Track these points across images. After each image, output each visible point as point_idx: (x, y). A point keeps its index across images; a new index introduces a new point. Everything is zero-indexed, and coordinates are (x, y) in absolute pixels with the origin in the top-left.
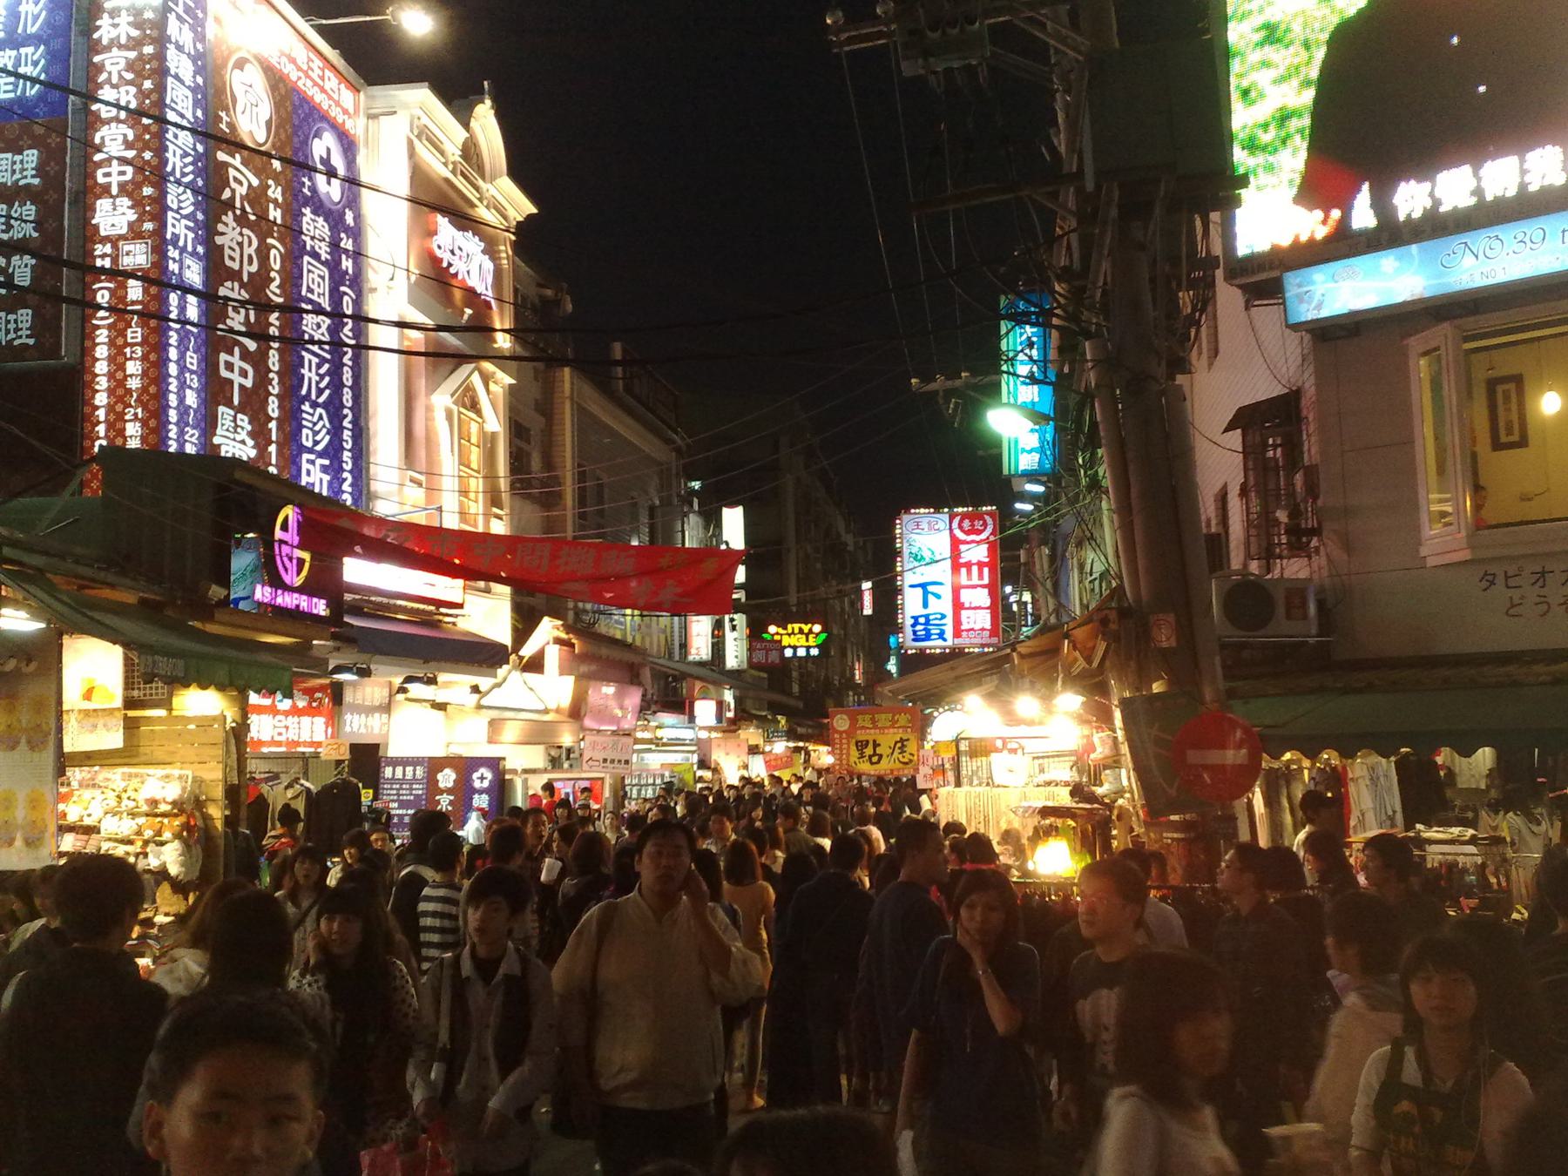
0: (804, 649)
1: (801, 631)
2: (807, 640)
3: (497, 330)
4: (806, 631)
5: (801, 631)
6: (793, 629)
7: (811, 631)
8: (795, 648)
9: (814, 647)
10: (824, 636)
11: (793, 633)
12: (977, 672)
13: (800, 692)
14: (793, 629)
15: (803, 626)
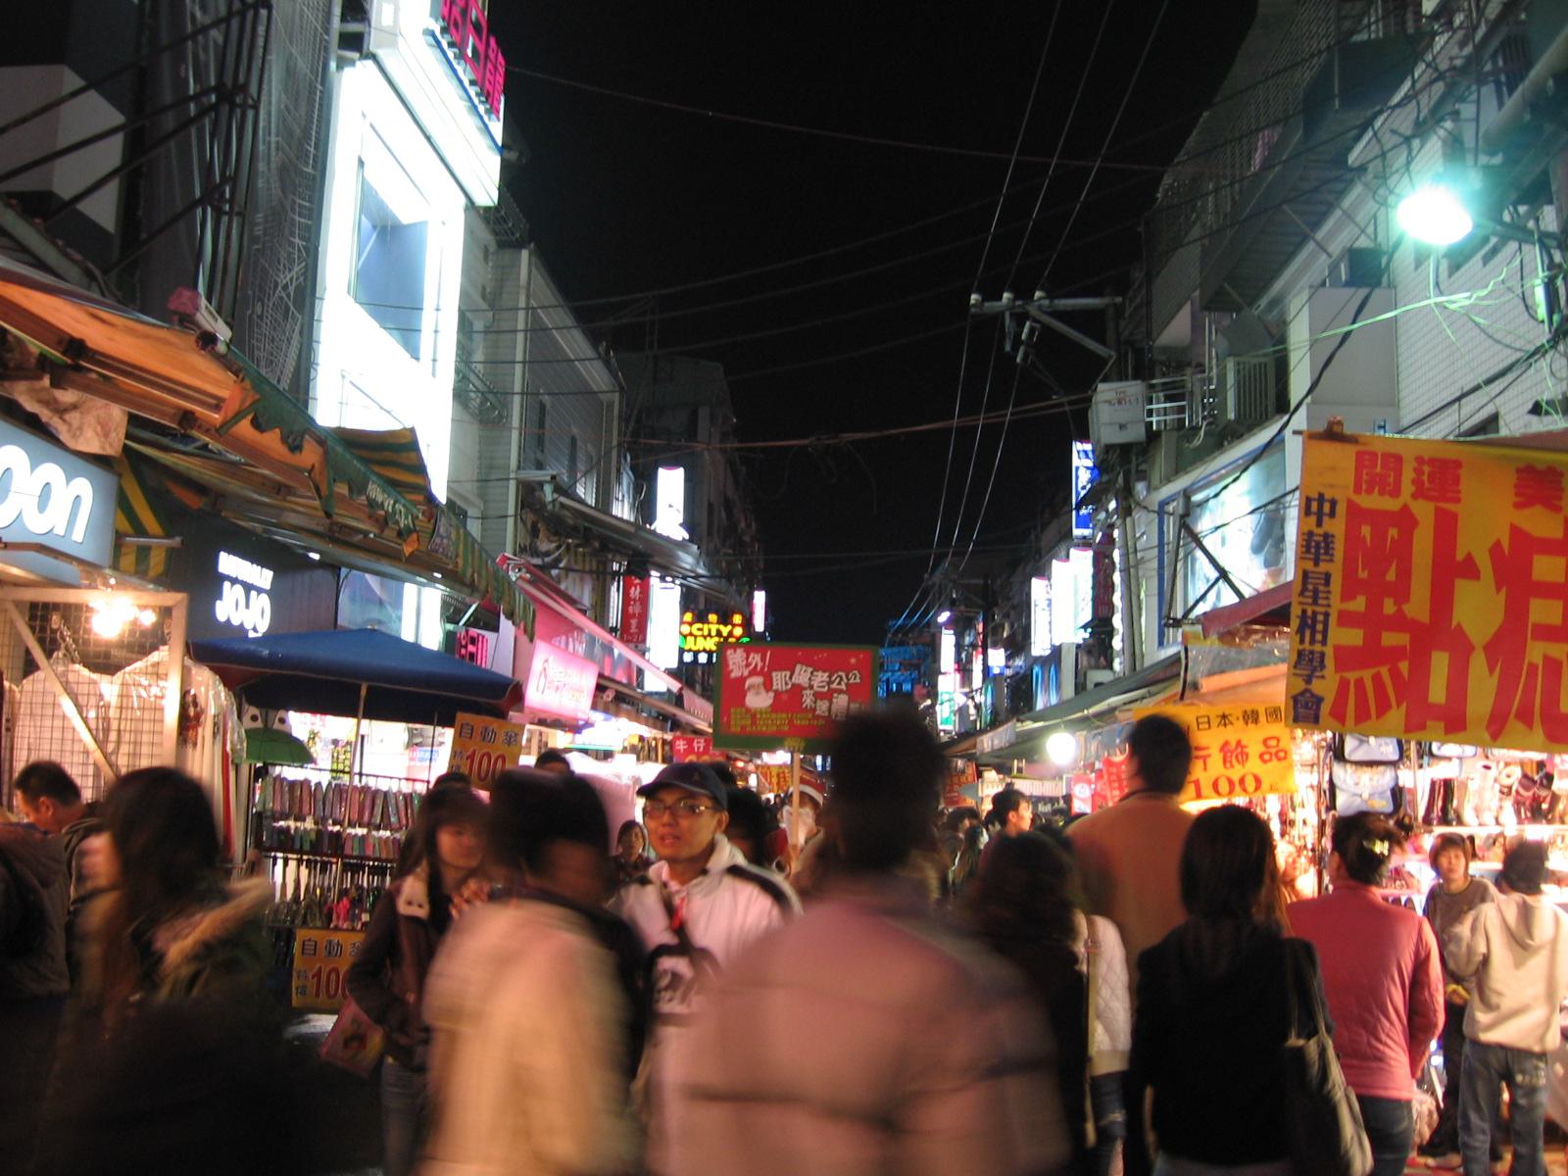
4: (725, 634)
6: (710, 630)
11: (710, 635)
14: (710, 630)
15: (722, 627)
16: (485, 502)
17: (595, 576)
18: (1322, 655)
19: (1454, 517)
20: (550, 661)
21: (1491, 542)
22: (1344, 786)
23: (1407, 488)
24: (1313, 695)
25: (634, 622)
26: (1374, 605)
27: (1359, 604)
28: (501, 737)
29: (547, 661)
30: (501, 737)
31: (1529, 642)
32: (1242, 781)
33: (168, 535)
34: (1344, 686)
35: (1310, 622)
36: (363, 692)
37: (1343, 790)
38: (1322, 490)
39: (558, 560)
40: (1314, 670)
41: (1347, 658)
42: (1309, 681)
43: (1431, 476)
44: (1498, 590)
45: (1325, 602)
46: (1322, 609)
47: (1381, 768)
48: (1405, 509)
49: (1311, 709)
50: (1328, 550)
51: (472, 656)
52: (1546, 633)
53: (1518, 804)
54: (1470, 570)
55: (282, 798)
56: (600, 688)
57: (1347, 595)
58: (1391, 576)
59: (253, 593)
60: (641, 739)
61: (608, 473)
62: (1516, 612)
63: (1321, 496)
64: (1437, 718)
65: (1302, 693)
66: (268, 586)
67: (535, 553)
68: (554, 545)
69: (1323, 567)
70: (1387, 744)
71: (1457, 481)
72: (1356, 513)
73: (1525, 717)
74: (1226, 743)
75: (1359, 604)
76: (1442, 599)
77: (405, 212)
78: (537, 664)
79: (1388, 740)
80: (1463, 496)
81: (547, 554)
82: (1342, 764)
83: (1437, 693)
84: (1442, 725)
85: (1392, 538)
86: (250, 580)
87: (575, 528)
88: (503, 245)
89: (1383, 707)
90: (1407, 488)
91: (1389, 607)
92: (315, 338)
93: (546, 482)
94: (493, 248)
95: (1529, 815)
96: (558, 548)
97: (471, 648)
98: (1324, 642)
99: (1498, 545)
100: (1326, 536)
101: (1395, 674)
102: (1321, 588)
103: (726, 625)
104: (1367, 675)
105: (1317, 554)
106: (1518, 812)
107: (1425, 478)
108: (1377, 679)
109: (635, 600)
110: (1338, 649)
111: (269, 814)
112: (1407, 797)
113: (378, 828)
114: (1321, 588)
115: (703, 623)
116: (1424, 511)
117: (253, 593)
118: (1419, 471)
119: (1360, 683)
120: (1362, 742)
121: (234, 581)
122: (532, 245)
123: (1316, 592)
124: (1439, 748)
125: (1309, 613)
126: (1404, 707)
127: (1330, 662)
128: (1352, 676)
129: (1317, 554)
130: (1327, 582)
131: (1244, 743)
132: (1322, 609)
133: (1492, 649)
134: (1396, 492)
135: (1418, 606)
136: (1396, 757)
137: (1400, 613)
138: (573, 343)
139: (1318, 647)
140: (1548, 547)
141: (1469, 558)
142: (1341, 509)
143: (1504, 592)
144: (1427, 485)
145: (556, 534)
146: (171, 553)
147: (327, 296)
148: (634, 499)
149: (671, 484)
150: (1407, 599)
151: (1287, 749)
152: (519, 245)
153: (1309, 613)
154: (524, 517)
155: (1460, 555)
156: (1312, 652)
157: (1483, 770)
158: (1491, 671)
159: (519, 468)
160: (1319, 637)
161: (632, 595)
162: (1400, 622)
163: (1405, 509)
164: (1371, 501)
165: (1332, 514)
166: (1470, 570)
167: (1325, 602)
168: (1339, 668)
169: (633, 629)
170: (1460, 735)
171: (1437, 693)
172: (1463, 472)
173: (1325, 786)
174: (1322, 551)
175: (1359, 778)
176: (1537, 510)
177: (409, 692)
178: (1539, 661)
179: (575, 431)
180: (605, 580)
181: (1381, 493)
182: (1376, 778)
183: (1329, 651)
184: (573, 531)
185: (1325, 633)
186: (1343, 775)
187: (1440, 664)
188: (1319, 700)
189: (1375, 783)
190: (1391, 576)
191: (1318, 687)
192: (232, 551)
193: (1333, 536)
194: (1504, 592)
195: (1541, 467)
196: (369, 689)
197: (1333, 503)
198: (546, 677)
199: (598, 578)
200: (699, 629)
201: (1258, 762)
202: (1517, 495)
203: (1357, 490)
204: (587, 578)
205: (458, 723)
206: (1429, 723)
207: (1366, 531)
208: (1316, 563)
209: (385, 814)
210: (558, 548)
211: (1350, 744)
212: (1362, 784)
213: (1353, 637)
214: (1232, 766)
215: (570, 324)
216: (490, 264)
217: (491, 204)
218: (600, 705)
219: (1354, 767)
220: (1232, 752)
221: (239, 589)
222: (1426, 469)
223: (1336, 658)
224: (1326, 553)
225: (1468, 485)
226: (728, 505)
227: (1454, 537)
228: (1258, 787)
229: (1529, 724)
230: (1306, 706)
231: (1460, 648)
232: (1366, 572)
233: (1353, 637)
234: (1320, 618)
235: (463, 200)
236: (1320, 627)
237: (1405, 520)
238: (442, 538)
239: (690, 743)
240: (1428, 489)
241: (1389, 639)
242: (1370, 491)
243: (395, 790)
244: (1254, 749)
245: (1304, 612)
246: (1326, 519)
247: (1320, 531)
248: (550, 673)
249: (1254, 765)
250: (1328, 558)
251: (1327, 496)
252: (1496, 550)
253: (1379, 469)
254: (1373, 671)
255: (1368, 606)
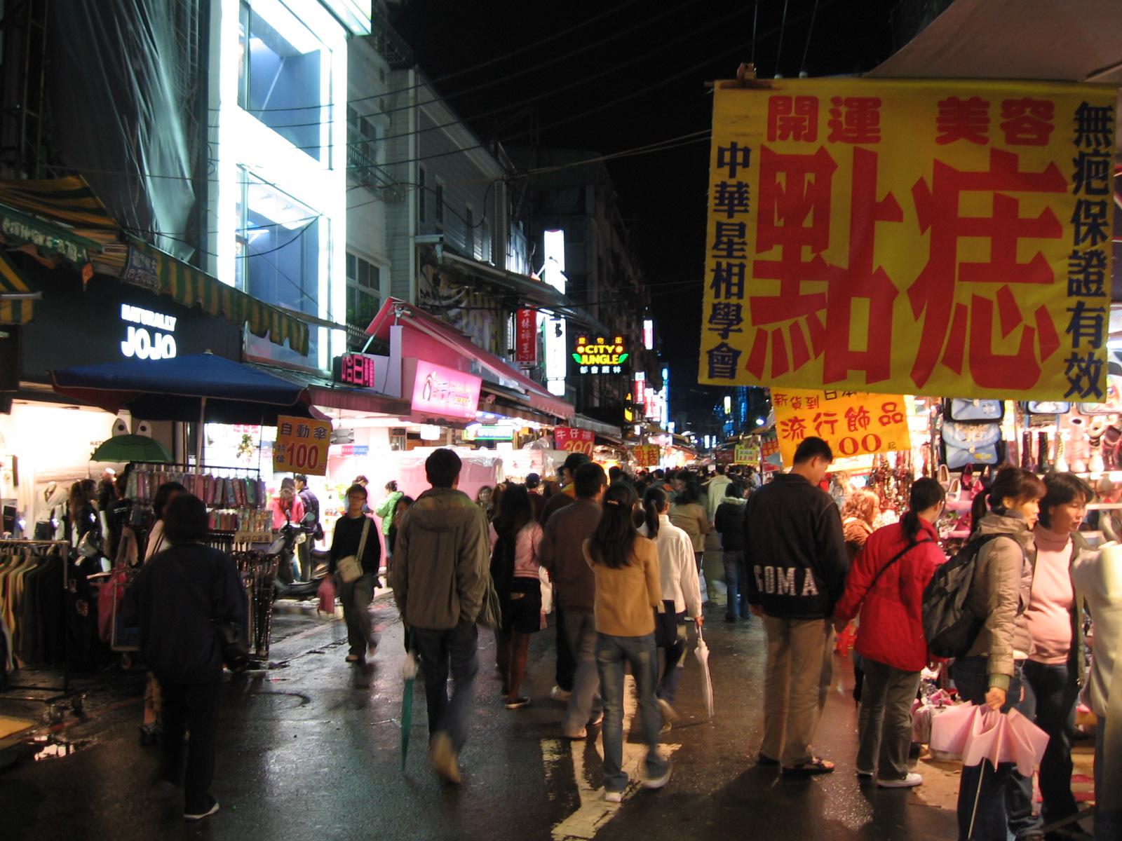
0: (586, 367)
1: (606, 352)
2: (611, 360)
3: (462, 150)
4: (610, 351)
5: (606, 352)
6: (599, 349)
7: (614, 352)
8: (600, 366)
9: (617, 365)
10: (624, 356)
11: (599, 353)
12: (153, 111)
13: (978, 471)
14: (599, 349)
15: (607, 347)
16: (393, 261)
17: (493, 312)
18: (739, 307)
19: (874, 156)
20: (434, 375)
21: (912, 182)
22: (953, 443)
23: (824, 131)
24: (730, 350)
25: (526, 345)
26: (792, 254)
27: (775, 254)
28: (313, 433)
29: (430, 376)
30: (313, 433)
31: (957, 283)
32: (864, 441)
33: (32, 291)
34: (761, 337)
35: (724, 274)
36: (203, 404)
37: (950, 445)
38: (735, 140)
39: (458, 303)
40: (731, 324)
41: (765, 309)
42: (725, 335)
43: (849, 116)
44: (923, 230)
45: (740, 254)
46: (737, 262)
47: (986, 426)
48: (822, 151)
49: (726, 363)
50: (743, 200)
51: (359, 374)
52: (973, 272)
53: (1107, 453)
54: (891, 211)
55: (144, 488)
56: (483, 395)
57: (763, 246)
58: (808, 223)
59: (158, 336)
60: (531, 430)
61: (500, 236)
62: (942, 252)
63: (734, 145)
64: (856, 367)
65: (718, 348)
66: (172, 328)
67: (436, 296)
68: (454, 291)
69: (738, 218)
70: (990, 405)
71: (876, 118)
72: (771, 163)
73: (954, 363)
74: (851, 410)
75: (775, 254)
76: (863, 247)
77: (301, 43)
78: (421, 377)
79: (991, 402)
80: (882, 134)
81: (449, 297)
82: (951, 423)
83: (858, 340)
84: (864, 373)
85: (809, 182)
86: (154, 325)
87: (469, 277)
88: (394, 68)
89: (801, 359)
90: (824, 131)
91: (807, 255)
92: (210, 139)
93: (437, 243)
94: (387, 70)
95: (1116, 461)
96: (459, 293)
97: (357, 368)
98: (740, 295)
99: (921, 182)
100: (740, 185)
101: (813, 322)
102: (736, 240)
103: (610, 345)
104: (785, 326)
105: (731, 205)
106: (1106, 459)
107: (842, 119)
108: (795, 329)
109: (526, 329)
110: (754, 300)
111: (135, 500)
112: (1009, 451)
113: (221, 507)
114: (736, 240)
115: (594, 345)
116: (842, 153)
117: (158, 336)
118: (835, 113)
119: (778, 334)
120: (968, 404)
121: (138, 326)
122: (417, 65)
123: (730, 243)
124: (1035, 406)
125: (724, 266)
126: (822, 356)
127: (746, 314)
128: (770, 328)
129: (731, 205)
130: (742, 235)
131: (865, 409)
132: (737, 262)
133: (916, 292)
134: (812, 137)
135: (838, 254)
136: (998, 416)
137: (819, 261)
138: (460, 137)
139: (734, 300)
140: (973, 181)
141: (890, 198)
142: (755, 157)
143: (929, 231)
144: (844, 126)
145: (457, 283)
146: (36, 303)
147: (222, 107)
148: (528, 255)
149: (554, 242)
150: (825, 245)
151: (902, 412)
152: (406, 67)
153: (724, 266)
154: (424, 270)
155: (880, 197)
156: (727, 306)
157: (1074, 424)
158: (917, 316)
159: (416, 234)
160: (735, 290)
161: (523, 326)
162: (817, 269)
163: (822, 151)
164: (787, 147)
165: (746, 164)
166: (891, 211)
167: (740, 254)
168: (755, 322)
169: (526, 351)
170: (882, 384)
171: (858, 340)
172: (882, 110)
173: (937, 442)
174: (736, 202)
175: (966, 435)
176: (962, 143)
177: (214, 400)
178: (967, 302)
179: (470, 206)
180: (502, 314)
181: (797, 138)
182: (982, 434)
183: (745, 303)
184: (468, 280)
185: (741, 285)
186: (954, 434)
187: (860, 312)
188: (737, 354)
189: (980, 439)
190: (808, 223)
191: (734, 341)
192: (133, 303)
193: (747, 186)
194: (929, 231)
195: (963, 98)
196: (208, 401)
197: (747, 151)
198: (430, 387)
199: (497, 314)
200: (591, 349)
201: (879, 424)
202: (940, 129)
203: (771, 138)
204: (486, 313)
205: (279, 422)
206: (850, 373)
207: (781, 178)
208: (730, 216)
209: (224, 496)
210: (459, 293)
211: (956, 406)
212: (968, 440)
213: (771, 288)
214: (856, 429)
215: (453, 121)
216: (386, 83)
217: (367, 34)
218: (486, 407)
219: (961, 427)
220: (856, 417)
221: (143, 333)
222: (843, 109)
223: (753, 311)
224: (740, 204)
225: (888, 122)
226: (616, 259)
227: (874, 178)
228: (878, 446)
229: (957, 368)
230: (723, 362)
231: (884, 295)
232: (782, 220)
233: (771, 288)
234: (735, 270)
235: (344, 33)
236: (735, 280)
237: (824, 164)
238: (136, 269)
239: (567, 431)
240: (846, 131)
241: (809, 288)
242: (784, 137)
243: (231, 478)
244: (875, 413)
245: (719, 264)
246: (739, 168)
247: (733, 182)
248: (435, 385)
249: (874, 427)
250: (742, 208)
251: (740, 146)
252: (919, 188)
253: (793, 114)
254: (790, 322)
255: (785, 254)
